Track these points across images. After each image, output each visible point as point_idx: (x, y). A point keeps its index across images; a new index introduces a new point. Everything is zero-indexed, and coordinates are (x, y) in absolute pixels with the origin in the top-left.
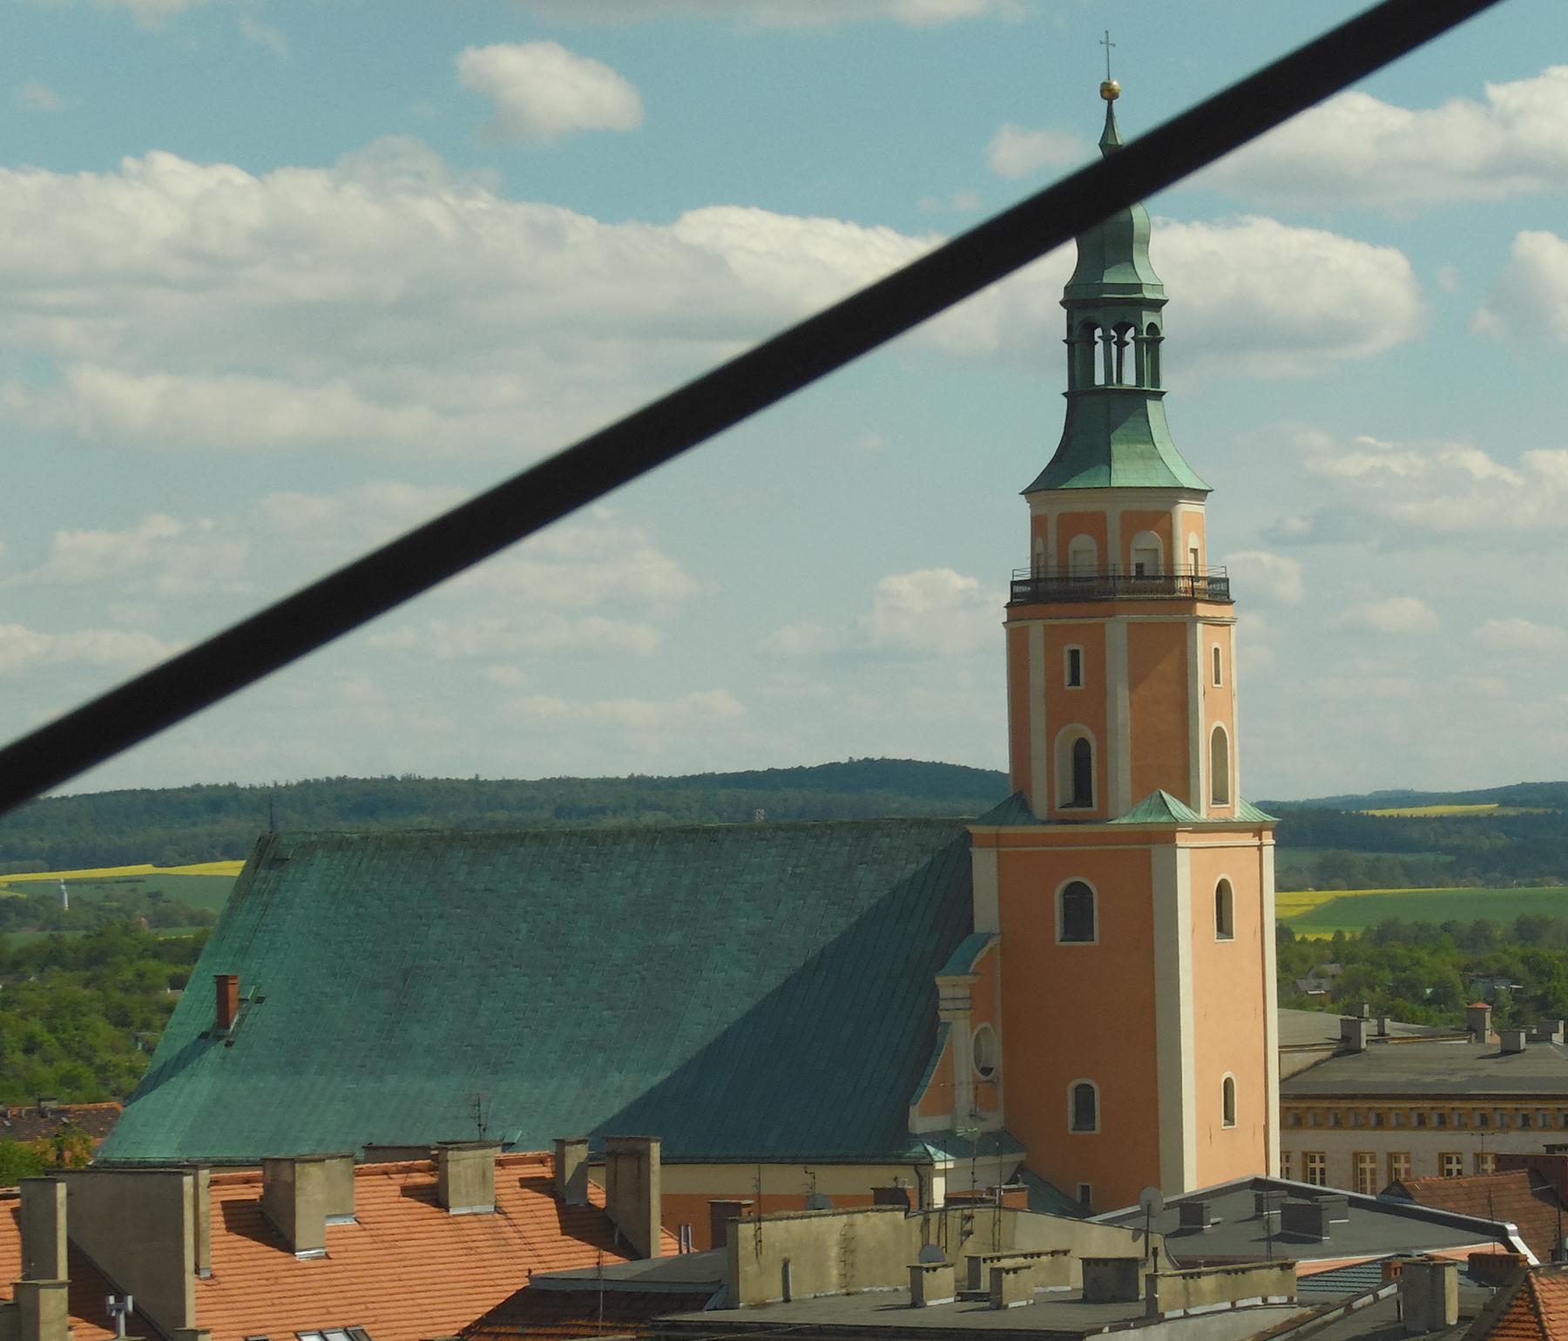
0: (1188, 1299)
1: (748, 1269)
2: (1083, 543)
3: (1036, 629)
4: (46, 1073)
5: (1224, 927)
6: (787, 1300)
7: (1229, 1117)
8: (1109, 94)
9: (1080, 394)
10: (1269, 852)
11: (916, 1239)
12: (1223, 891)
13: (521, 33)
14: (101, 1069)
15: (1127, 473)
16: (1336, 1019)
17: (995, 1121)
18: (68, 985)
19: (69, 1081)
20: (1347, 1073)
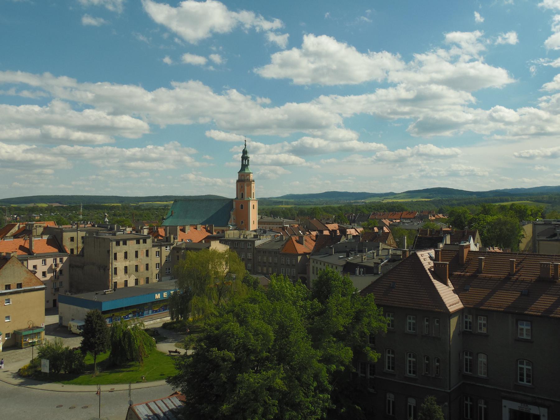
0: (263, 238)
1: (226, 235)
2: (243, 177)
3: (239, 184)
4: (146, 219)
5: (254, 208)
6: (124, 234)
7: (254, 224)
8: (245, 141)
9: (242, 165)
10: (257, 202)
11: (239, 233)
12: (254, 205)
13: (542, 85)
14: (151, 218)
15: (246, 171)
16: (260, 216)
17: (235, 224)
18: (148, 211)
19: (149, 219)
20: (262, 220)
